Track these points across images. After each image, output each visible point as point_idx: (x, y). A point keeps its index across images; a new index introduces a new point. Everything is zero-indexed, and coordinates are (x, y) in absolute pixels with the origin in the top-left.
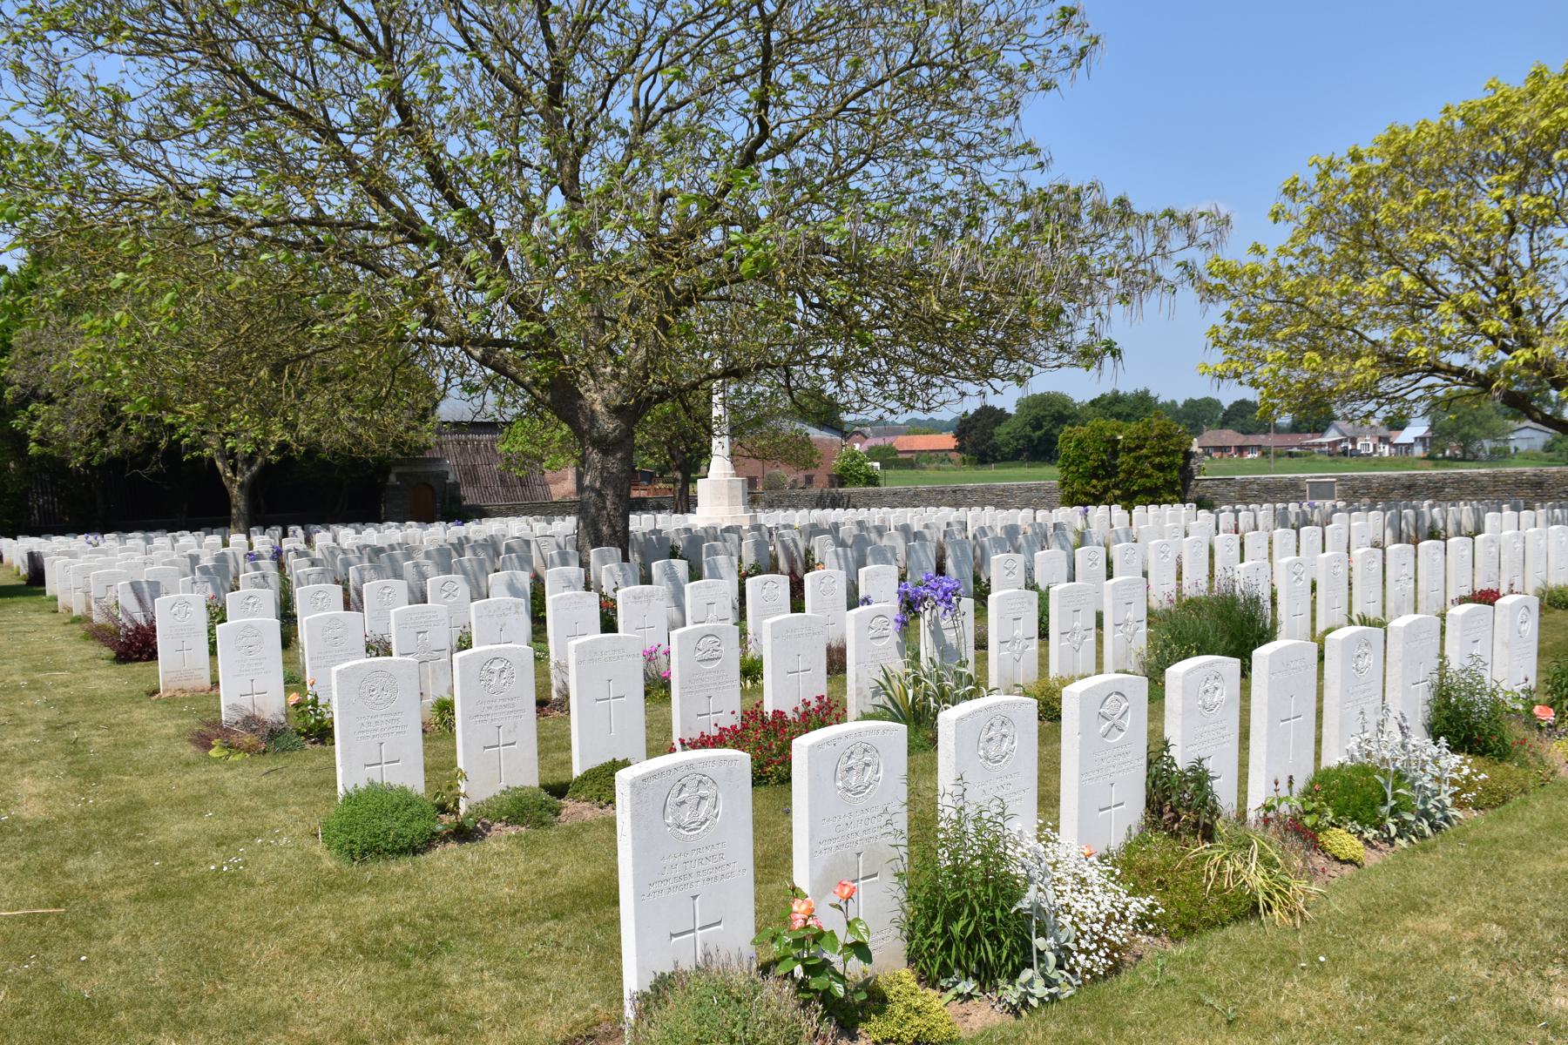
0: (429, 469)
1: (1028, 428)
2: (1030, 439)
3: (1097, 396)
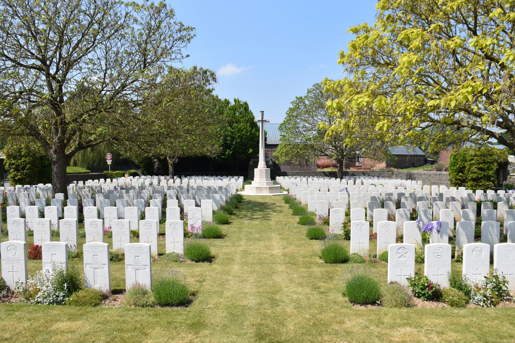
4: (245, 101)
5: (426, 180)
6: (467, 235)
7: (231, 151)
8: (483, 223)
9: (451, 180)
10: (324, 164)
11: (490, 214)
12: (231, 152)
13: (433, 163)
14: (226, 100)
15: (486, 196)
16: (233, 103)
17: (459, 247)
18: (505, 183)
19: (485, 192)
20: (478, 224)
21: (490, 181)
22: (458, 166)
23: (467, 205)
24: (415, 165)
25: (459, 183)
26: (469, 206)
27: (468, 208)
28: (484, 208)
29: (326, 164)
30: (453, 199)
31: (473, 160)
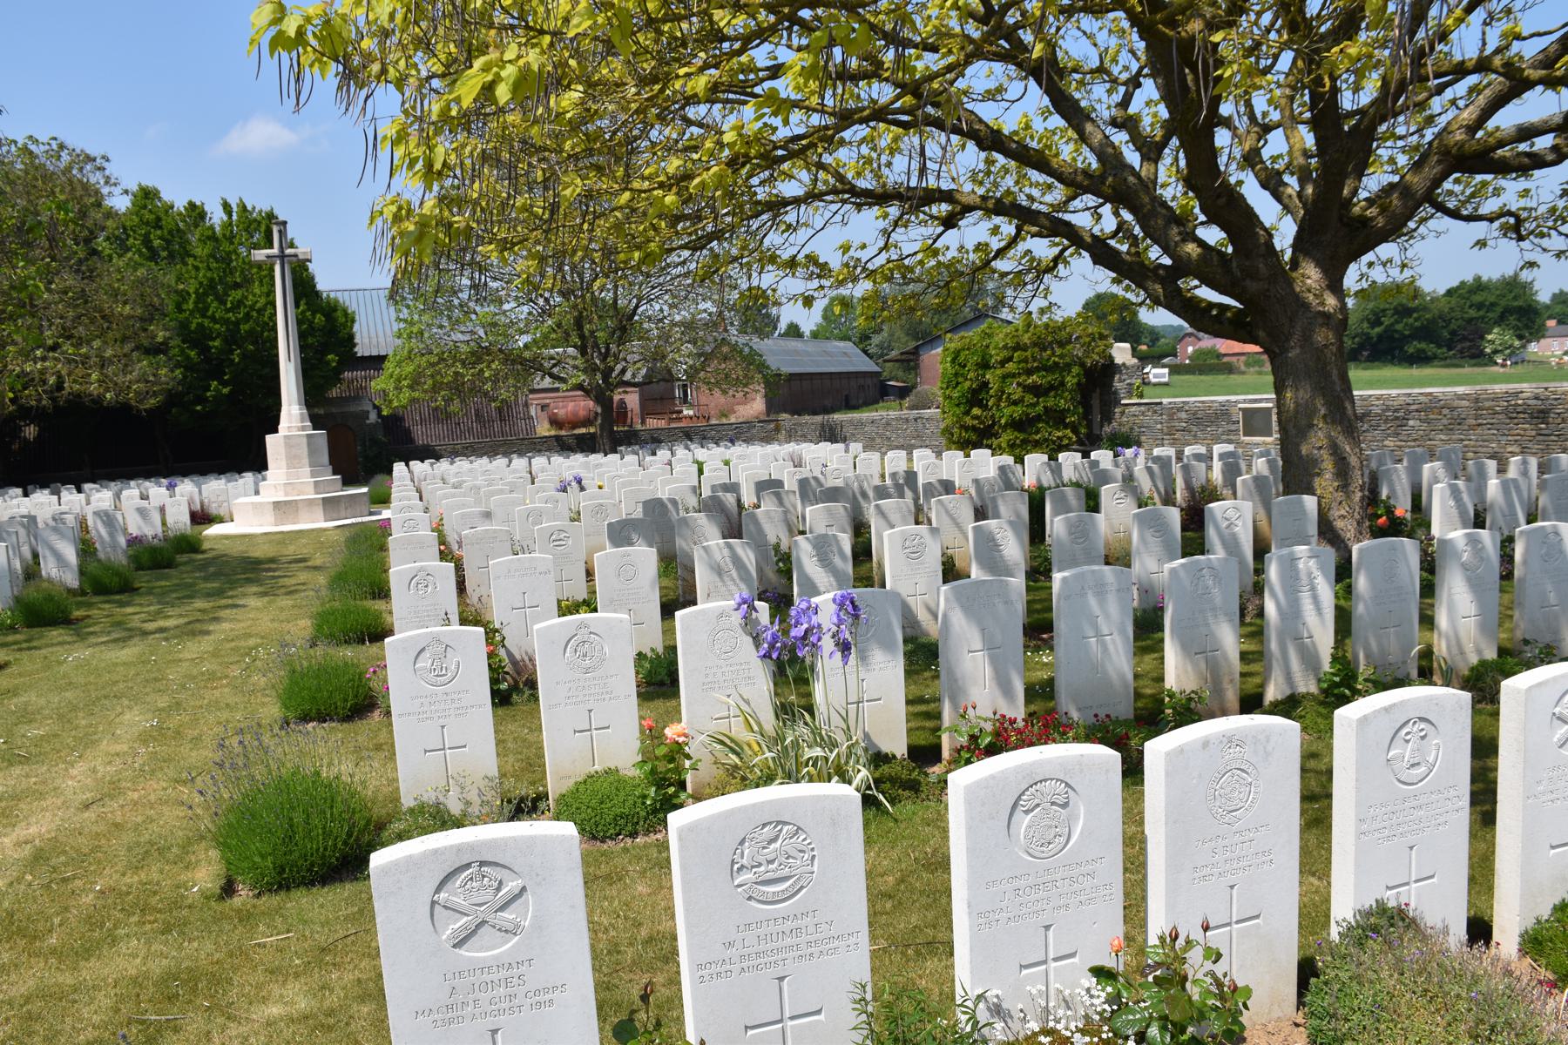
0: (346, 409)
1: (1365, 325)
2: (1368, 337)
3: (1455, 284)
4: (266, 208)
5: (878, 441)
6: (990, 646)
7: (225, 384)
8: (1057, 577)
9: (947, 432)
10: (575, 414)
11: (1080, 533)
12: (226, 391)
13: (903, 393)
14: (192, 206)
15: (1057, 471)
16: (217, 216)
17: (955, 705)
18: (1107, 429)
19: (1053, 458)
20: (1039, 572)
21: (1066, 427)
22: (968, 384)
23: (996, 507)
24: (853, 402)
25: (971, 438)
26: (1002, 509)
27: (997, 516)
28: (1056, 513)
29: (582, 413)
30: (948, 487)
31: (1010, 359)
